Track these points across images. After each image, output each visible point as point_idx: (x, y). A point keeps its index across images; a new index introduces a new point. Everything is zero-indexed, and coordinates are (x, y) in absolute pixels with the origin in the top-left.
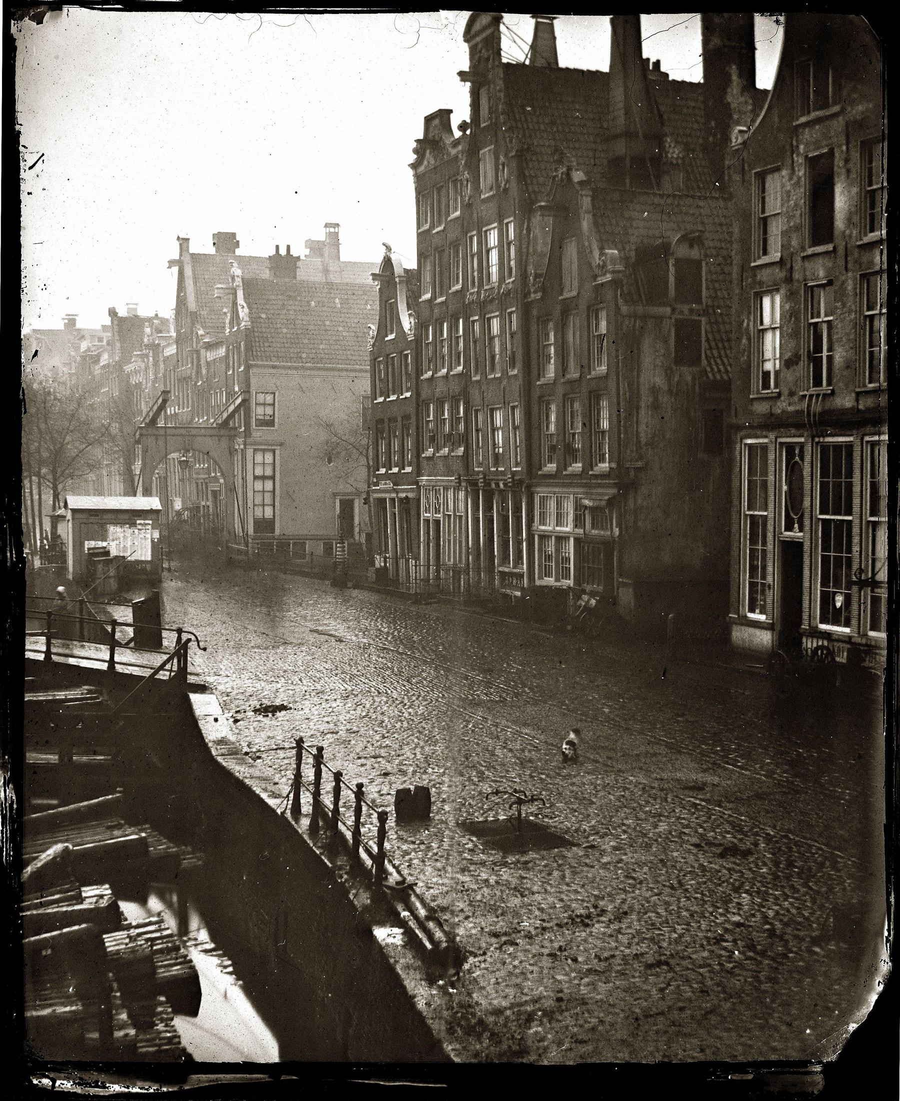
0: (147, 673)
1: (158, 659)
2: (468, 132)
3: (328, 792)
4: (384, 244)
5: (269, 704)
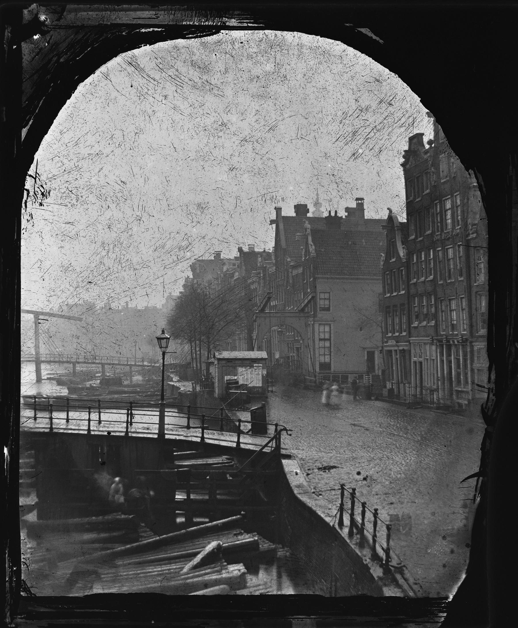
0: (258, 449)
1: (263, 441)
2: (433, 145)
3: (359, 514)
4: (388, 209)
5: (326, 465)
